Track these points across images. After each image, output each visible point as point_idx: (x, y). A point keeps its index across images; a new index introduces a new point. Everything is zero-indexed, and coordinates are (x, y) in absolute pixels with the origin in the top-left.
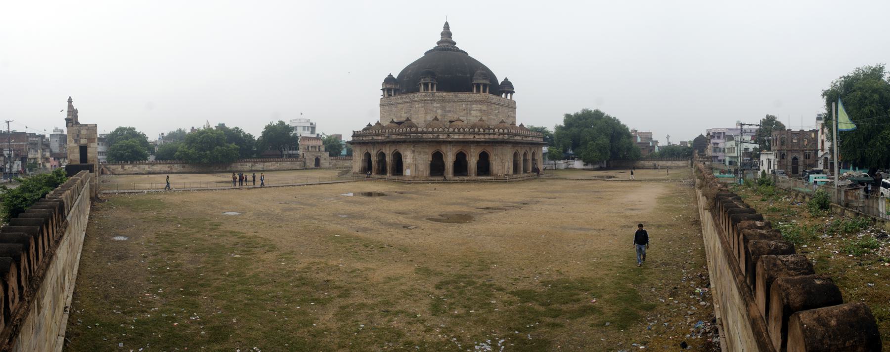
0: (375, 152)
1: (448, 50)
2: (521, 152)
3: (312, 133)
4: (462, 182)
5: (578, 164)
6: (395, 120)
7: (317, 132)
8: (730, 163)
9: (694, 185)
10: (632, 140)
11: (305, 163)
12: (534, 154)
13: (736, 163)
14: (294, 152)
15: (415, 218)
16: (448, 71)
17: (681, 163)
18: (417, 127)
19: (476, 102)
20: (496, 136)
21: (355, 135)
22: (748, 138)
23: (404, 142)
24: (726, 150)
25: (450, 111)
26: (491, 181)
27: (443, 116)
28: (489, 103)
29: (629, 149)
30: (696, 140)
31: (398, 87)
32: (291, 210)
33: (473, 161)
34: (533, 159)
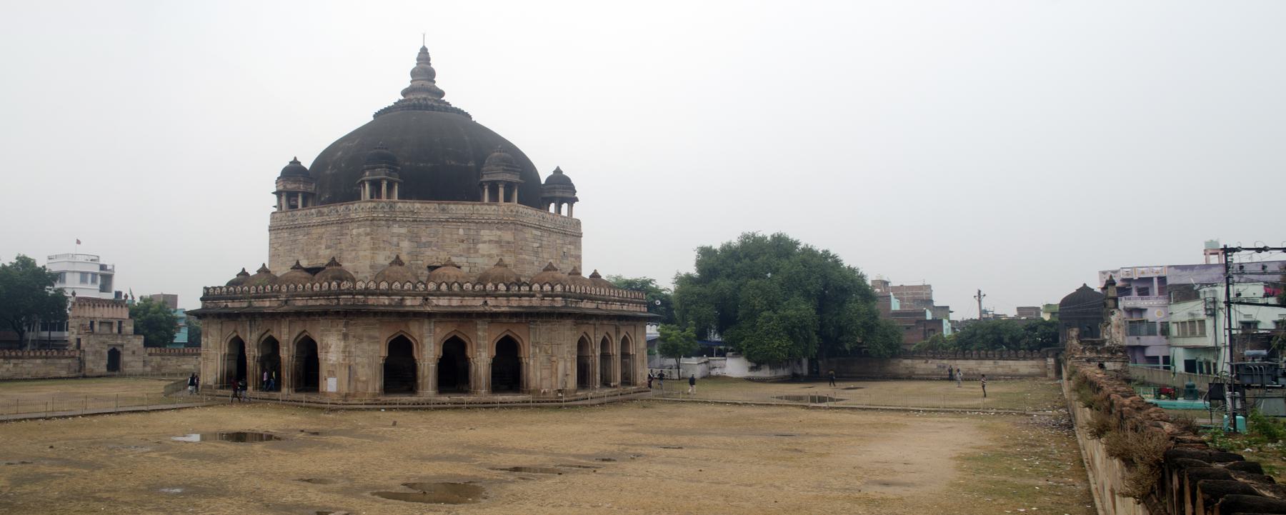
0: (255, 337)
1: (427, 107)
2: (596, 337)
3: (105, 287)
4: (457, 407)
5: (734, 367)
6: (304, 263)
7: (118, 285)
8: (1190, 366)
9: (1070, 426)
10: (878, 306)
11: (82, 363)
12: (625, 342)
13: (1210, 368)
14: (55, 334)
15: (346, 492)
16: (423, 155)
17: (1024, 366)
18: (354, 280)
19: (488, 223)
20: (536, 302)
21: (209, 295)
22: (1256, 291)
23: (324, 313)
24: (1174, 330)
25: (429, 244)
26: (525, 406)
27: (414, 255)
28: (517, 225)
29: (871, 326)
30: (1067, 302)
31: (311, 188)
32: (37, 479)
33: (482, 359)
34: (625, 355)
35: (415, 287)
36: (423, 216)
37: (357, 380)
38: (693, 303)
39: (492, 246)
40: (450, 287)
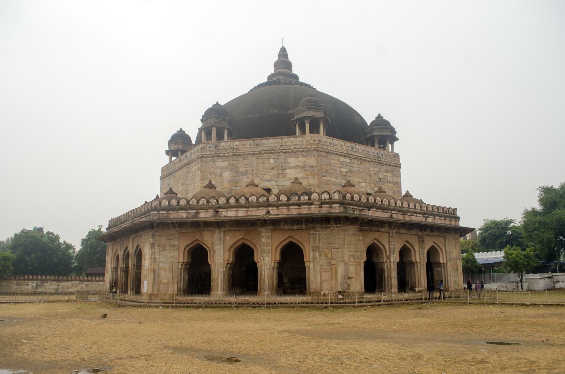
19: (294, 152)
25: (246, 173)
26: (304, 306)
33: (267, 263)
35: (208, 202)
36: (241, 151)
37: (160, 283)
38: (535, 229)
39: (299, 170)
40: (237, 200)
